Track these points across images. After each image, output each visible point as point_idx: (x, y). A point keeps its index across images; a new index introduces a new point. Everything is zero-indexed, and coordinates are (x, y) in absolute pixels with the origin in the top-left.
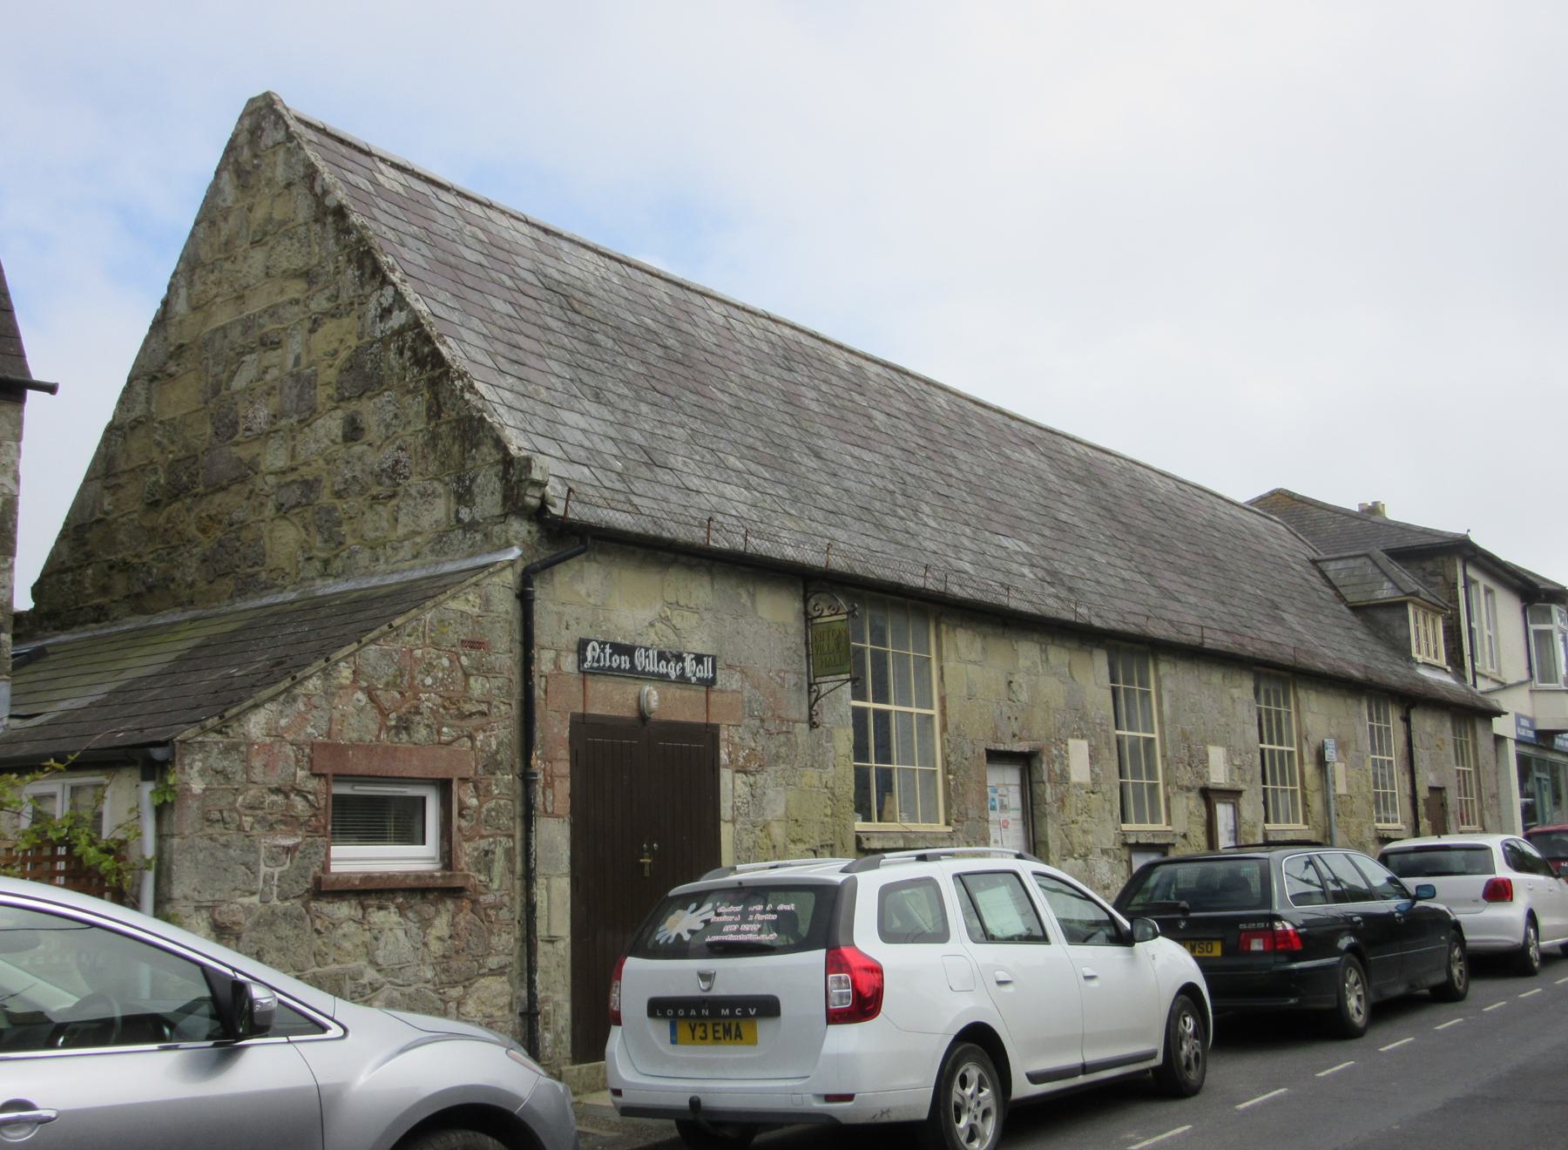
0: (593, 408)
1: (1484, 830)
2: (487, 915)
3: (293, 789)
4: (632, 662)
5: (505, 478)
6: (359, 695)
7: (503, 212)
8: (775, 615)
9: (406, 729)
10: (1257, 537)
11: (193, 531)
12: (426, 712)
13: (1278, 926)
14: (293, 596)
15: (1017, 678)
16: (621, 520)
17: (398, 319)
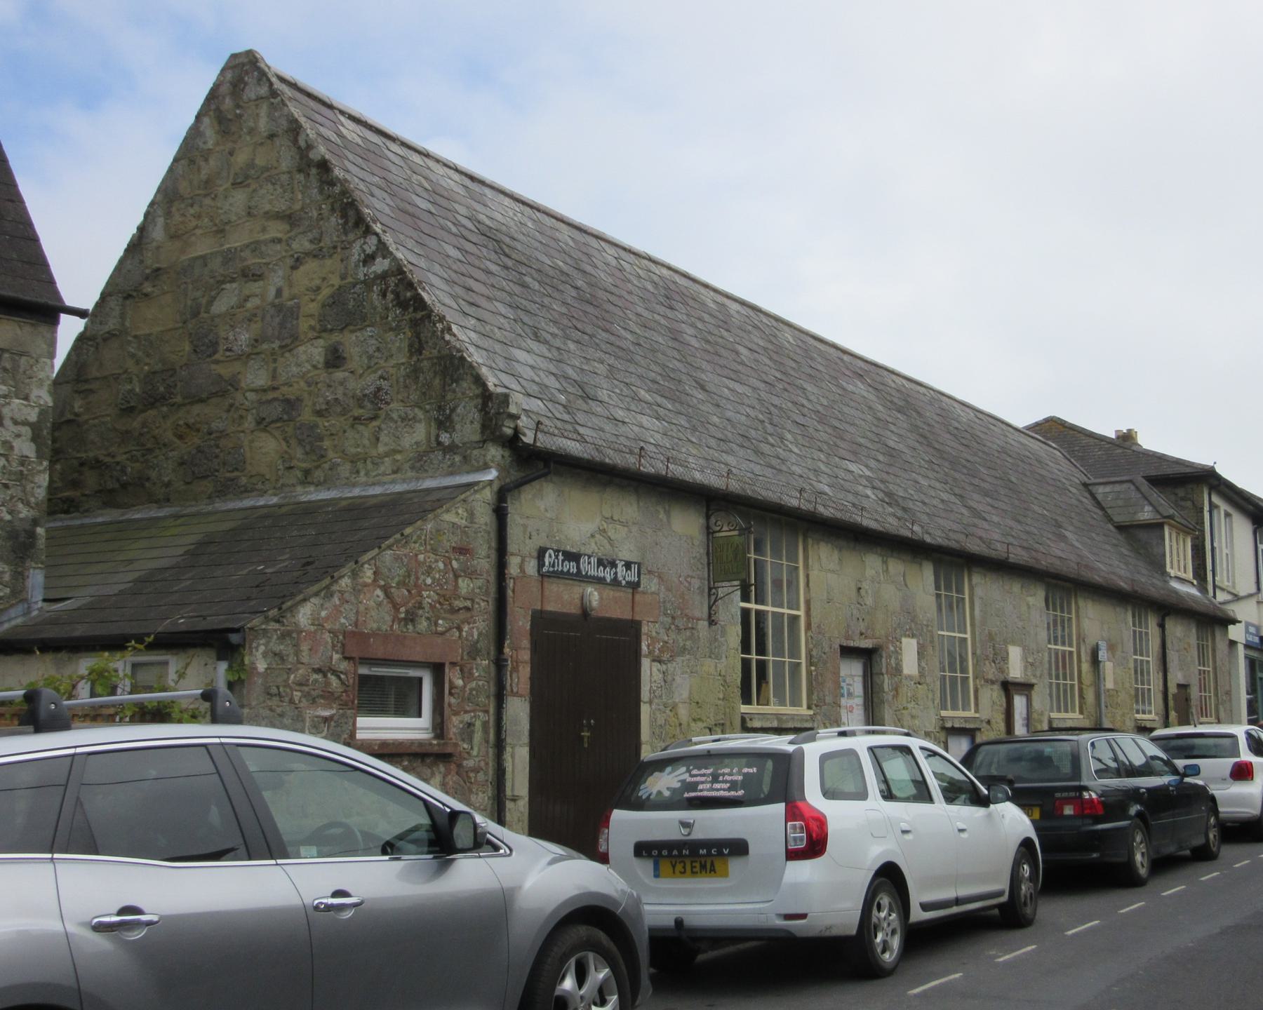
0: (534, 345)
1: (1219, 722)
2: (469, 777)
3: (330, 669)
4: (578, 567)
5: (483, 409)
6: (379, 592)
7: (438, 161)
8: (685, 526)
9: (412, 621)
10: (1040, 462)
11: (169, 436)
12: (427, 608)
13: (1086, 795)
14: (275, 500)
15: (865, 585)
16: (572, 447)
17: (381, 265)
